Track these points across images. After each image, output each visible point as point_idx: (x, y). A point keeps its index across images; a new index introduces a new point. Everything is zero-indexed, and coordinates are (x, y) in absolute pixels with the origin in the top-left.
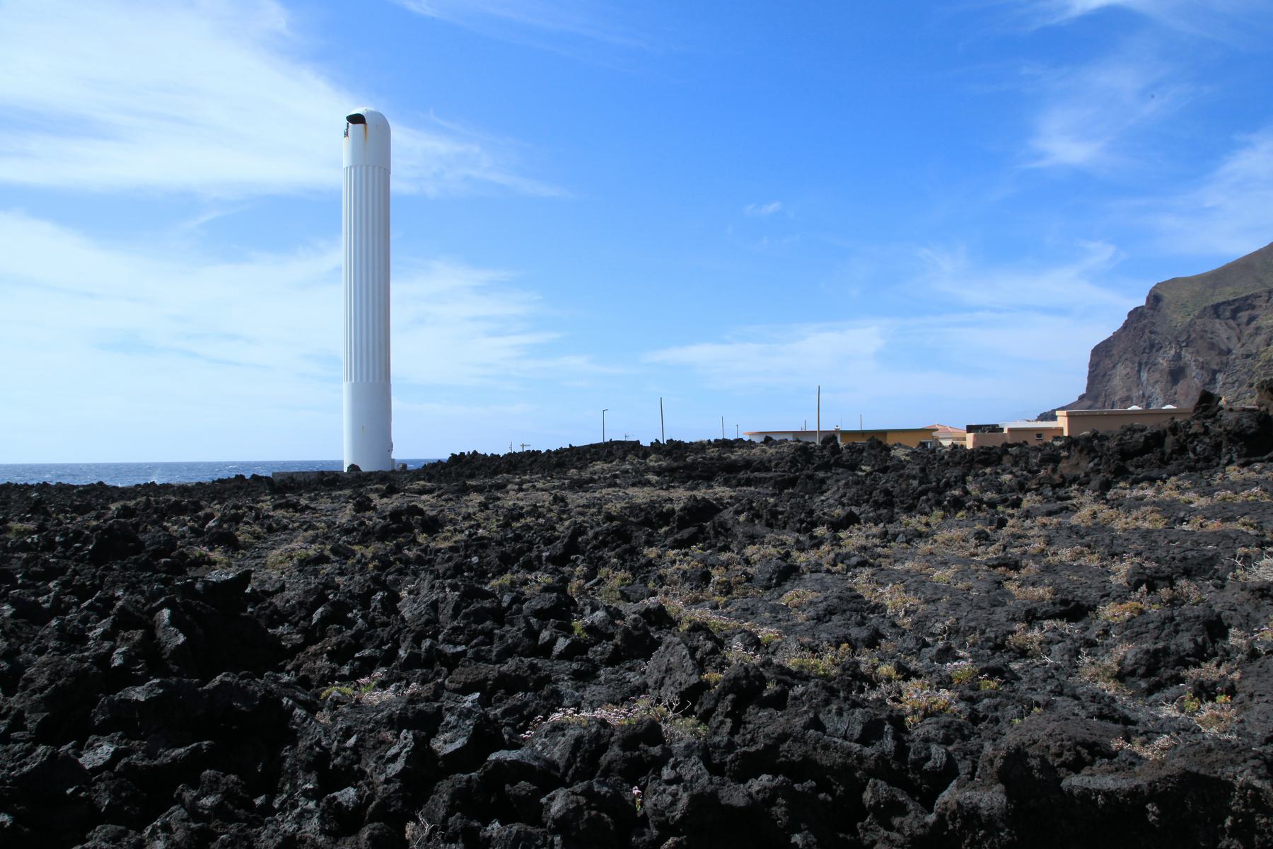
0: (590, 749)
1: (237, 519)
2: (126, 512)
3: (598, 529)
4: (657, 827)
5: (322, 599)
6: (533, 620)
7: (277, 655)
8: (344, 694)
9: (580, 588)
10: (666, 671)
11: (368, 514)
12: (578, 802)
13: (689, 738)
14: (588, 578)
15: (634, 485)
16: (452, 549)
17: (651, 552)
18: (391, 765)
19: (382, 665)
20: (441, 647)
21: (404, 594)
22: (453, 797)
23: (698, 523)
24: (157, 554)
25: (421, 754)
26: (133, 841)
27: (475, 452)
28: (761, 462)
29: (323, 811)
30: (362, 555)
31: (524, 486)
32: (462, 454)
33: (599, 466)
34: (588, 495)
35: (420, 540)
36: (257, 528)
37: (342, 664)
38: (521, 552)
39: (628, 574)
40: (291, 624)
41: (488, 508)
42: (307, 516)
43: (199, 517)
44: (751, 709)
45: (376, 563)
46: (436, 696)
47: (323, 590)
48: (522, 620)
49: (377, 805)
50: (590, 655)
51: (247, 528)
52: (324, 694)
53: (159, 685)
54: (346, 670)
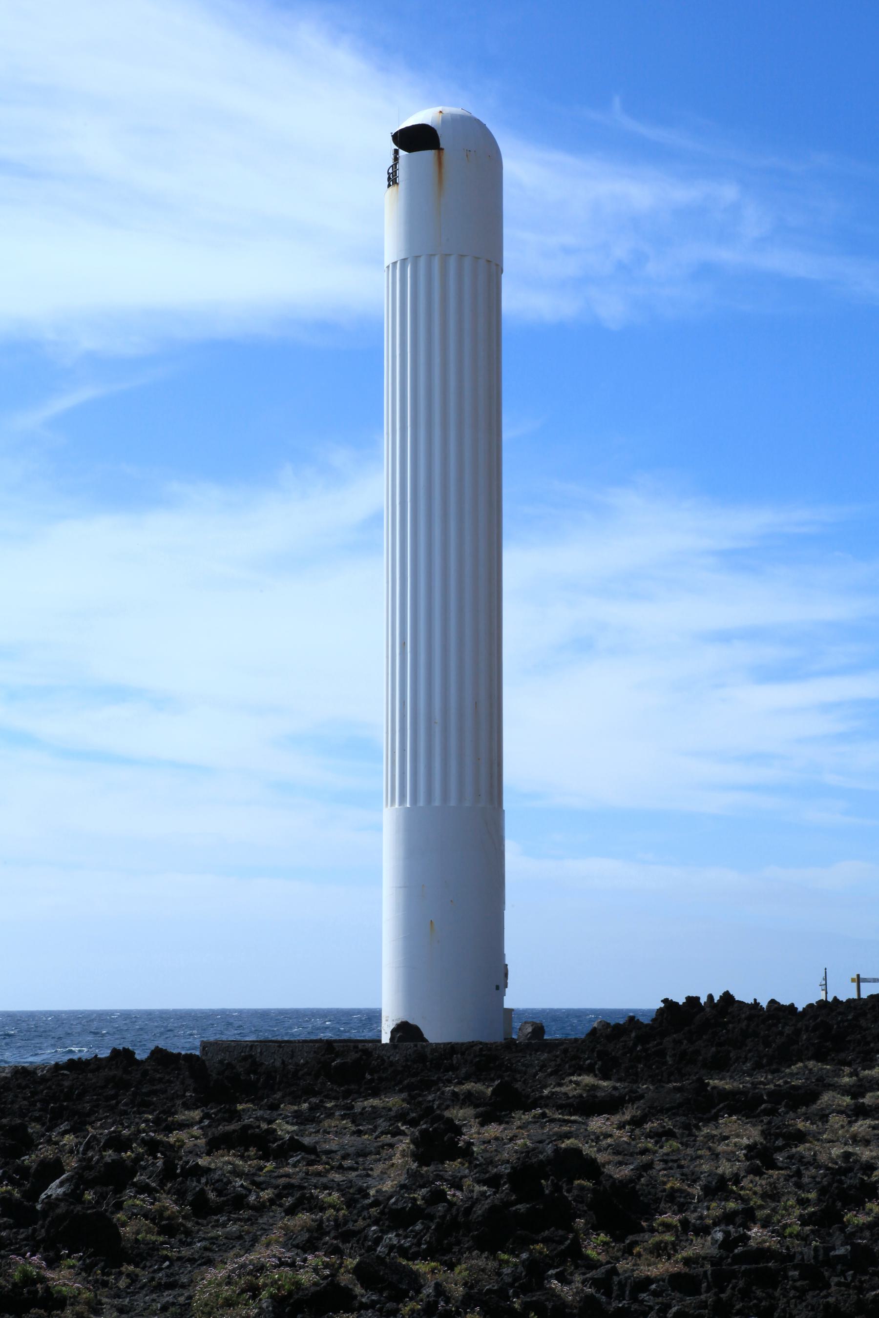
1: (118, 1177)
11: (452, 1167)
16: (677, 1282)
27: (727, 997)
32: (692, 1001)
35: (591, 1253)
36: (169, 1203)
42: (293, 1169)
43: (24, 1171)
51: (142, 1201)
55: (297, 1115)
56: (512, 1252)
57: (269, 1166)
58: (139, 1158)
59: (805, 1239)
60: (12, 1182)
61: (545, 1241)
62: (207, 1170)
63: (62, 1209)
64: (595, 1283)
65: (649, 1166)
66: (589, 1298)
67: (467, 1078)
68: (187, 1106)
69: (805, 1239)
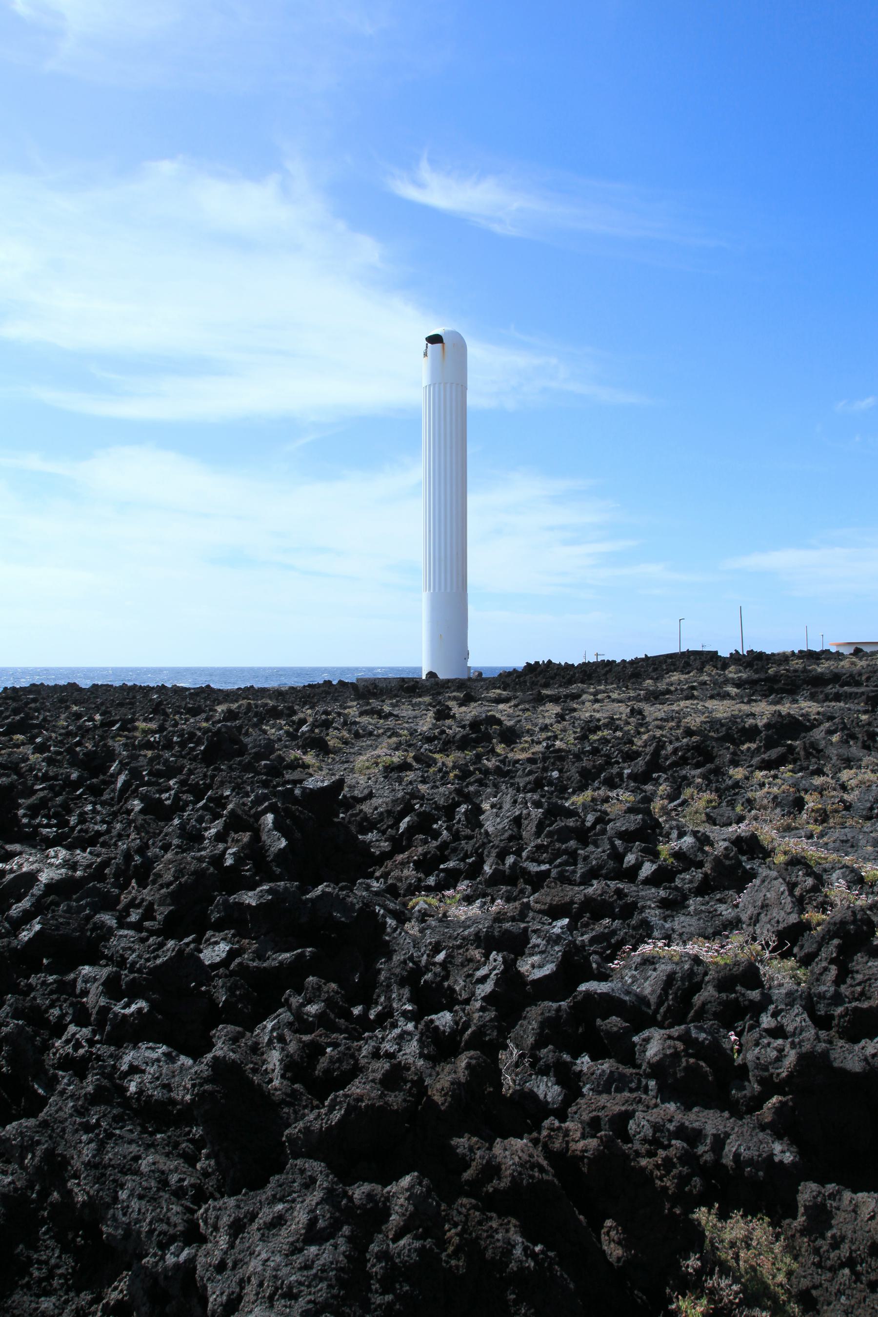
0: (684, 985)
1: (327, 724)
2: (231, 715)
3: (677, 744)
4: (759, 1083)
5: (408, 809)
6: (618, 842)
7: (365, 863)
8: (430, 905)
9: (663, 808)
10: (762, 907)
11: (448, 722)
12: (675, 1048)
13: (789, 985)
14: (672, 798)
15: (712, 697)
17: (738, 773)
18: (480, 986)
19: (466, 878)
20: (525, 865)
21: (486, 806)
22: (543, 1025)
23: (784, 742)
24: (258, 757)
25: (510, 977)
26: (250, 1043)
27: (550, 662)
28: (851, 676)
29: (422, 1034)
30: (443, 764)
31: (599, 697)
32: (537, 663)
33: (676, 677)
34: (666, 708)
36: (345, 734)
37: (428, 874)
38: (601, 769)
39: (714, 796)
40: (379, 831)
41: (564, 720)
42: (390, 722)
43: (293, 722)
44: (859, 957)
45: (457, 772)
46: (522, 916)
47: (409, 800)
48: (606, 841)
49: (473, 1032)
50: (678, 882)
51: (336, 732)
52: (411, 904)
53: (269, 892)
54: (431, 881)
55: (391, 704)
56: (470, 751)
57: (382, 721)
58: (334, 718)
59: (575, 745)
60: (289, 725)
61: (482, 747)
62: (359, 723)
63: (307, 735)
64: (500, 761)
65: (520, 721)
66: (498, 766)
67: (454, 691)
68: (351, 701)
69: (575, 745)
